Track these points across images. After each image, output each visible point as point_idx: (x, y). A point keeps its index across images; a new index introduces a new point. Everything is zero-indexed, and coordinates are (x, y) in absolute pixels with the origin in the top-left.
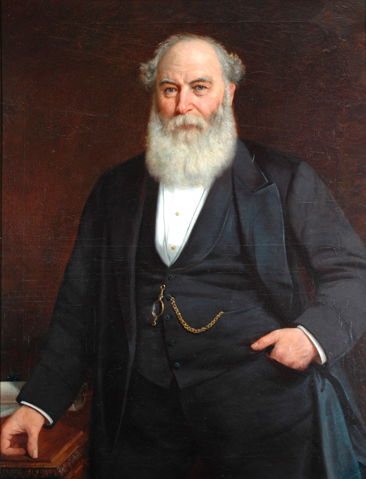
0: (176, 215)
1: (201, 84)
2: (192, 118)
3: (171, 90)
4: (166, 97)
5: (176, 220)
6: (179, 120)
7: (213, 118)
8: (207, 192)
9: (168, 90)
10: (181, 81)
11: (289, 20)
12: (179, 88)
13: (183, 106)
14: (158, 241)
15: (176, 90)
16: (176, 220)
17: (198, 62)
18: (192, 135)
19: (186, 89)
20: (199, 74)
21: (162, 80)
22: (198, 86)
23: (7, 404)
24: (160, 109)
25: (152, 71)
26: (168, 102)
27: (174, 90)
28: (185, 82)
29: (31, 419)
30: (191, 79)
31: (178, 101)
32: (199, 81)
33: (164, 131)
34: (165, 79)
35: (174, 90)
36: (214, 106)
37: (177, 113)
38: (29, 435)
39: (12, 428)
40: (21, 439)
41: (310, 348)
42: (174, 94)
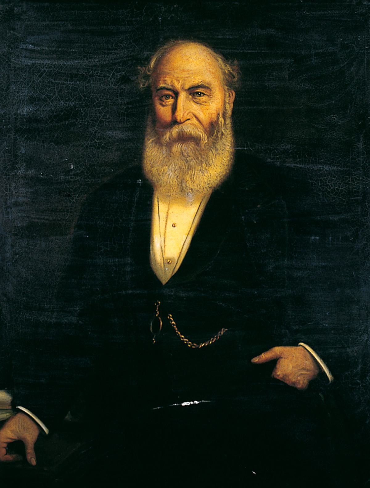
0: (172, 226)
1: (199, 90)
2: (189, 128)
3: (168, 97)
4: (163, 106)
5: (172, 232)
6: (175, 131)
7: (212, 128)
8: (205, 204)
9: (164, 98)
10: (178, 86)
11: (326, 170)
12: (176, 94)
13: (180, 115)
14: (154, 255)
15: (173, 97)
16: (172, 232)
17: (194, 68)
18: (188, 148)
19: (183, 96)
20: (196, 80)
21: (157, 87)
22: (195, 92)
23: (158, 202)
24: (156, 119)
25: (147, 77)
26: (164, 111)
27: (171, 98)
28: (183, 88)
29: (26, 427)
30: (187, 87)
31: (174, 108)
32: (198, 87)
33: (158, 142)
34: (162, 85)
35: (171, 98)
36: (214, 116)
37: (175, 122)
38: (23, 440)
39: (9, 433)
40: (16, 446)
41: (309, 363)
42: (171, 101)
